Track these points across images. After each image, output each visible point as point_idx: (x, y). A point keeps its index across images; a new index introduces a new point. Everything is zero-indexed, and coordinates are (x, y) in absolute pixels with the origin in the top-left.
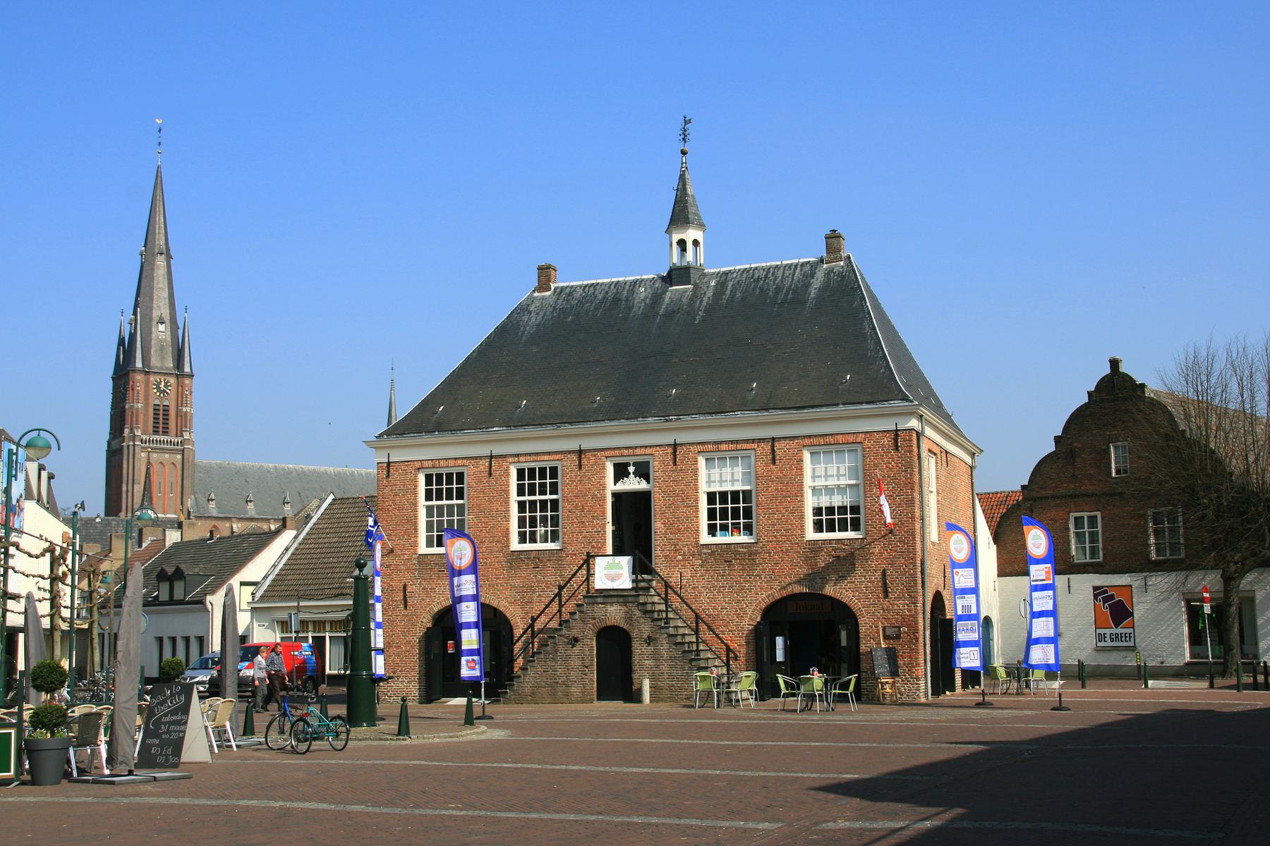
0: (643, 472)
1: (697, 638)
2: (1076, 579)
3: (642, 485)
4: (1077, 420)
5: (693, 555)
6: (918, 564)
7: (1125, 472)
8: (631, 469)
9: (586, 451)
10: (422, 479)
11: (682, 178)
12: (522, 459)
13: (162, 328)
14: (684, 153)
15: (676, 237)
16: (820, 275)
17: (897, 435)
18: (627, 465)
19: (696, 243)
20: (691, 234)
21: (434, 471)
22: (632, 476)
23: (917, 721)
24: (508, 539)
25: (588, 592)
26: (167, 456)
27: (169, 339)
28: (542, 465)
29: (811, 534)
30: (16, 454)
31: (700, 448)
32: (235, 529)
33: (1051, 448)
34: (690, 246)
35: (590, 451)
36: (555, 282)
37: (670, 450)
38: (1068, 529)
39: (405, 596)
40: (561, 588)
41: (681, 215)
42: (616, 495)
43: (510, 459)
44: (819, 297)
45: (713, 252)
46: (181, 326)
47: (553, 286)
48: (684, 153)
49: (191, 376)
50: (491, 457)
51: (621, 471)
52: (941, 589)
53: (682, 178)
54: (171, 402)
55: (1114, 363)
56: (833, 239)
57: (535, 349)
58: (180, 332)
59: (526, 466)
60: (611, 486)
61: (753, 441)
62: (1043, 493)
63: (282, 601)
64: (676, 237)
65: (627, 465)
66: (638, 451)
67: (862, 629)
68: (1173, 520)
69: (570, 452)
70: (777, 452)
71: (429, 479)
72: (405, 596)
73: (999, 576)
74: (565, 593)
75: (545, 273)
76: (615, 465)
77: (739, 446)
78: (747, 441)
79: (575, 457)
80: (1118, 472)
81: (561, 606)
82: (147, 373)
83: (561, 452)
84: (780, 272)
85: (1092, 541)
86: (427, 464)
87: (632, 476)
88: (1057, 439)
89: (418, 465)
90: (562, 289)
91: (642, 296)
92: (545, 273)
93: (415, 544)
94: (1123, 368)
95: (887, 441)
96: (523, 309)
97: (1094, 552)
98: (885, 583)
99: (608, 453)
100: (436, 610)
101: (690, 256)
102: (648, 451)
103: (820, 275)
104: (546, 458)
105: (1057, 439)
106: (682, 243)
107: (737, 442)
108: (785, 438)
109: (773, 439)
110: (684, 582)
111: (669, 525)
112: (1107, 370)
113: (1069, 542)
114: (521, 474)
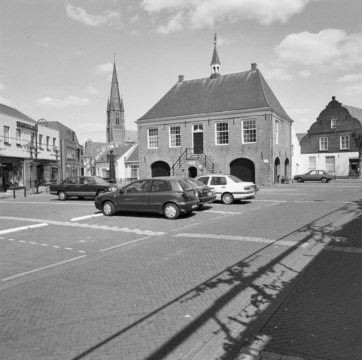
0: (201, 128)
1: (213, 170)
2: (320, 154)
3: (201, 131)
4: (323, 113)
5: (213, 149)
6: (271, 150)
7: (335, 127)
8: (198, 127)
9: (187, 122)
10: (148, 131)
11: (215, 51)
12: (172, 125)
13: (117, 100)
14: (215, 44)
15: (213, 66)
16: (250, 74)
17: (266, 116)
18: (197, 126)
19: (218, 68)
20: (216, 66)
21: (151, 129)
22: (198, 128)
23: (263, 192)
24: (169, 145)
25: (187, 158)
26: (116, 129)
27: (118, 103)
28: (176, 126)
29: (243, 143)
30: (37, 125)
31: (215, 121)
32: (126, 145)
33: (316, 121)
34: (216, 69)
35: (188, 122)
36: (183, 80)
37: (208, 122)
38: (319, 142)
39: (145, 159)
40: (180, 157)
41: (215, 60)
42: (194, 134)
43: (169, 125)
44: (249, 80)
45: (226, 70)
46: (121, 100)
47: (183, 81)
48: (215, 44)
49: (124, 111)
50: (164, 125)
51: (196, 128)
52: (279, 157)
53: (215, 51)
54: (119, 117)
55: (334, 98)
56: (254, 65)
57: (177, 97)
58: (121, 101)
59: (173, 127)
60: (193, 131)
61: (229, 119)
62: (313, 133)
63: (131, 161)
64: (213, 66)
65: (197, 126)
66: (200, 122)
67: (256, 167)
68: (347, 138)
69: (183, 123)
70: (235, 121)
71: (150, 130)
72: (145, 159)
73: (302, 153)
74: (181, 158)
75: (181, 77)
76: (194, 126)
77: (225, 120)
78: (227, 119)
79: (184, 124)
80: (333, 127)
81: (180, 162)
82: (113, 111)
83: (181, 123)
84: (239, 74)
85: (325, 145)
86: (149, 127)
87: (198, 128)
88: (317, 119)
89: (147, 127)
90: (185, 81)
91: (204, 82)
92: (181, 77)
93: (147, 147)
94: (336, 99)
95: (263, 118)
96: (175, 87)
97: (326, 147)
98: (262, 155)
99: (192, 123)
100: (152, 163)
101: (216, 71)
102: (202, 122)
103: (250, 74)
104: (177, 124)
105: (317, 119)
106: (214, 68)
107: (224, 119)
108: (237, 118)
109: (234, 118)
110: (211, 155)
111: (208, 141)
112: (331, 100)
113: (319, 145)
114: (171, 128)
